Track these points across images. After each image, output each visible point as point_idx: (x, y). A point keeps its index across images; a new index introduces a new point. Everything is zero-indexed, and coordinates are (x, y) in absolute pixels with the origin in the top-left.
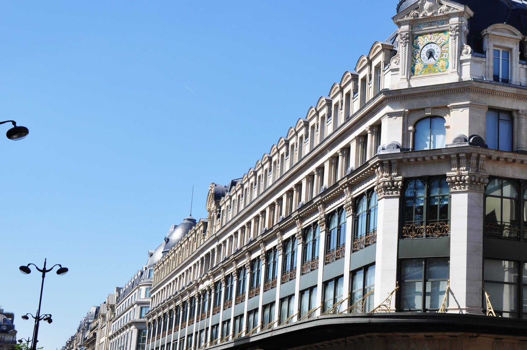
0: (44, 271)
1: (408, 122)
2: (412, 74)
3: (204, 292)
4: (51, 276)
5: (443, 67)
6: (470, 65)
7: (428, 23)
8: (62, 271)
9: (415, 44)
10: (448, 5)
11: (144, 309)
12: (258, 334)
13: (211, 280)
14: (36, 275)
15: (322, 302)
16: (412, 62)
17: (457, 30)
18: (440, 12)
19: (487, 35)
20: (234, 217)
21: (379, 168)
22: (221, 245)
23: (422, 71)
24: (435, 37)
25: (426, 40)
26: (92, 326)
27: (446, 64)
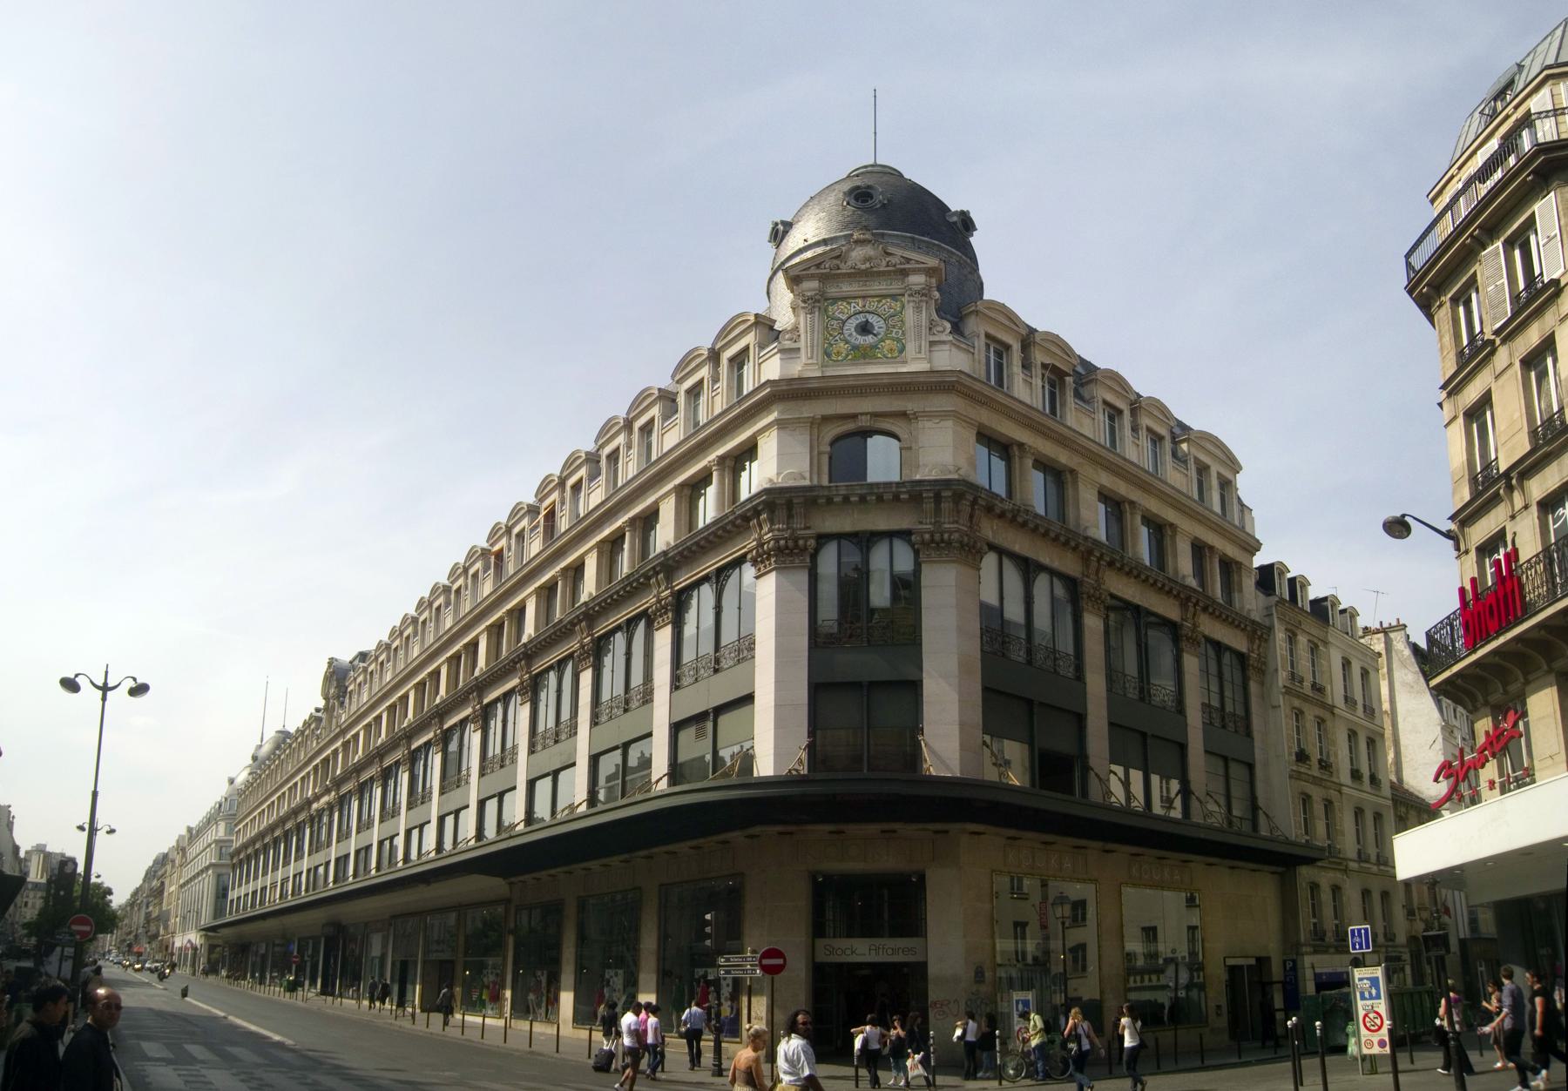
0: (105, 689)
3: (320, 812)
4: (118, 697)
8: (139, 690)
11: (224, 850)
12: (546, 825)
13: (333, 793)
14: (89, 695)
15: (526, 812)
18: (888, 266)
20: (397, 675)
21: (523, 662)
22: (348, 742)
23: (847, 355)
26: (160, 873)
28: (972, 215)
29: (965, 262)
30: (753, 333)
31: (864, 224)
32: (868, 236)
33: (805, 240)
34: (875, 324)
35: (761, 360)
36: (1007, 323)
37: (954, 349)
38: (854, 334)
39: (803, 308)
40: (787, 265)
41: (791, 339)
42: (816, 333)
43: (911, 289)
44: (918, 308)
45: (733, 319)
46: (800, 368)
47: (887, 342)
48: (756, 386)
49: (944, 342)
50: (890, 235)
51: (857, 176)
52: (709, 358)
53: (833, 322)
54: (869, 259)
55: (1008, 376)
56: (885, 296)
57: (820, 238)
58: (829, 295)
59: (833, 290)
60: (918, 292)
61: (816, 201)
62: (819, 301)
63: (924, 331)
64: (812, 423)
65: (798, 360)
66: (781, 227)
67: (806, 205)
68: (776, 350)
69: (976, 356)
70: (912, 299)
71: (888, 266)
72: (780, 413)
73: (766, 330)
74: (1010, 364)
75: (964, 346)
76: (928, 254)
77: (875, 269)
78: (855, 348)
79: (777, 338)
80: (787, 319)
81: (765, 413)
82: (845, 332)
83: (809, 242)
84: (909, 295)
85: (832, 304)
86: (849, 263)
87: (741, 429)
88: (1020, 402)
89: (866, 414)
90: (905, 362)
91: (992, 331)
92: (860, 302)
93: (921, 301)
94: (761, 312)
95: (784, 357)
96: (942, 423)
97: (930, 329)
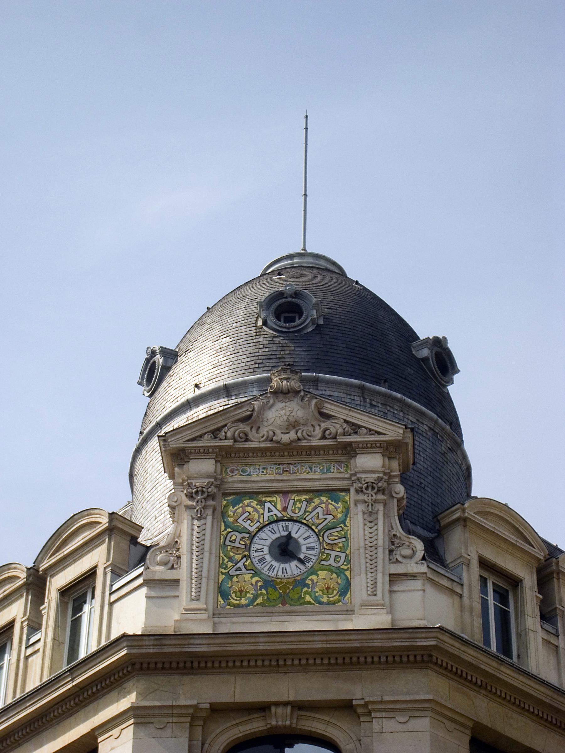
1: (208, 741)
2: (222, 602)
5: (330, 591)
6: (190, 722)
7: (279, 464)
9: (231, 520)
10: (348, 419)
16: (220, 566)
17: (378, 490)
18: (324, 437)
19: (462, 522)
23: (256, 597)
24: (298, 505)
25: (270, 510)
27: (340, 581)
28: (451, 346)
29: (443, 429)
30: (104, 546)
31: (289, 360)
32: (294, 384)
33: (197, 386)
34: (301, 541)
35: (114, 597)
36: (513, 538)
37: (430, 590)
38: (268, 558)
39: (188, 507)
40: (168, 428)
41: (165, 564)
42: (206, 555)
43: (359, 479)
44: (371, 513)
45: (73, 519)
46: (177, 617)
47: (322, 574)
48: (103, 643)
49: (413, 576)
50: (328, 382)
51: (279, 272)
52: (27, 586)
53: (240, 556)
54: (293, 425)
55: (519, 635)
56: (319, 492)
57: (221, 384)
58: (229, 487)
59: (237, 478)
60: (371, 486)
61: (214, 317)
62: (212, 496)
63: (380, 556)
64: (193, 717)
65: (175, 602)
66: (159, 360)
67: (200, 322)
68: (140, 581)
69: (465, 599)
70: (361, 497)
71: (324, 437)
72: (141, 695)
73: (125, 544)
74: (520, 613)
75: (445, 582)
76: (385, 416)
77: (304, 443)
78: (269, 584)
79: (142, 560)
80: (159, 526)
81: (114, 694)
82: (254, 554)
83: (203, 390)
84: (357, 491)
85: (234, 504)
86: (264, 431)
87: (72, 719)
88: (542, 682)
89: (285, 704)
90: (350, 612)
91: (491, 555)
92: (279, 500)
93: (376, 501)
94: (117, 507)
95: (153, 594)
96: (413, 721)
97: (391, 551)
